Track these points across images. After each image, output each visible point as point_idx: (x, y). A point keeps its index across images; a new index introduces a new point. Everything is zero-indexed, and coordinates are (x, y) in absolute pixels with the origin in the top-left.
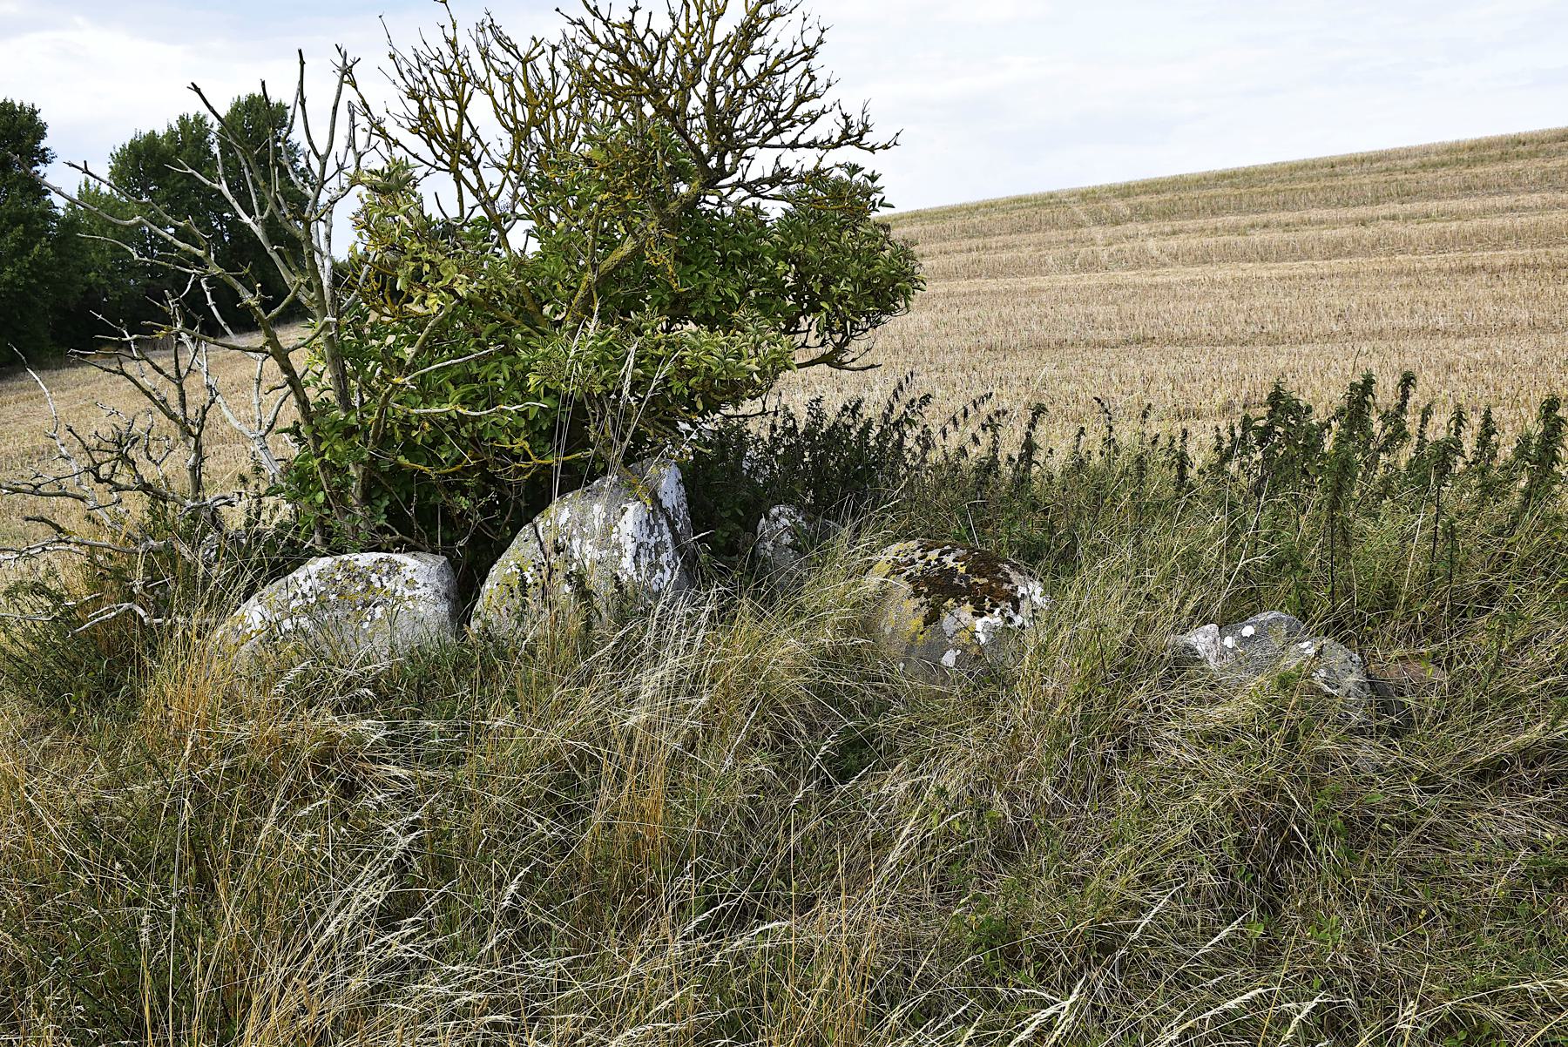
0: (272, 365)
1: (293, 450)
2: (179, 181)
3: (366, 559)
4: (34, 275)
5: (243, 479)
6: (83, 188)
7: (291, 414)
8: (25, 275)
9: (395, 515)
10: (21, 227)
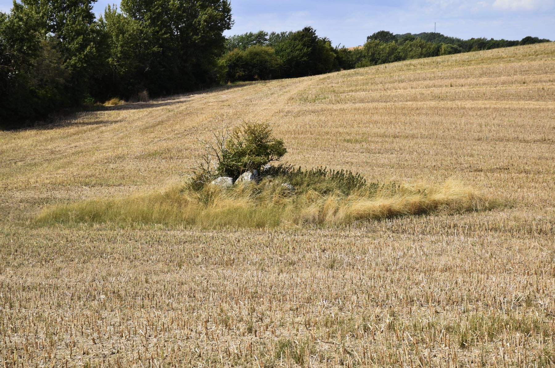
0: (217, 157)
1: (218, 166)
2: (157, 9)
3: (225, 178)
4: (85, 62)
5: (520, 157)
6: (107, 11)
7: (218, 162)
8: (81, 61)
9: (228, 173)
10: (82, 37)
